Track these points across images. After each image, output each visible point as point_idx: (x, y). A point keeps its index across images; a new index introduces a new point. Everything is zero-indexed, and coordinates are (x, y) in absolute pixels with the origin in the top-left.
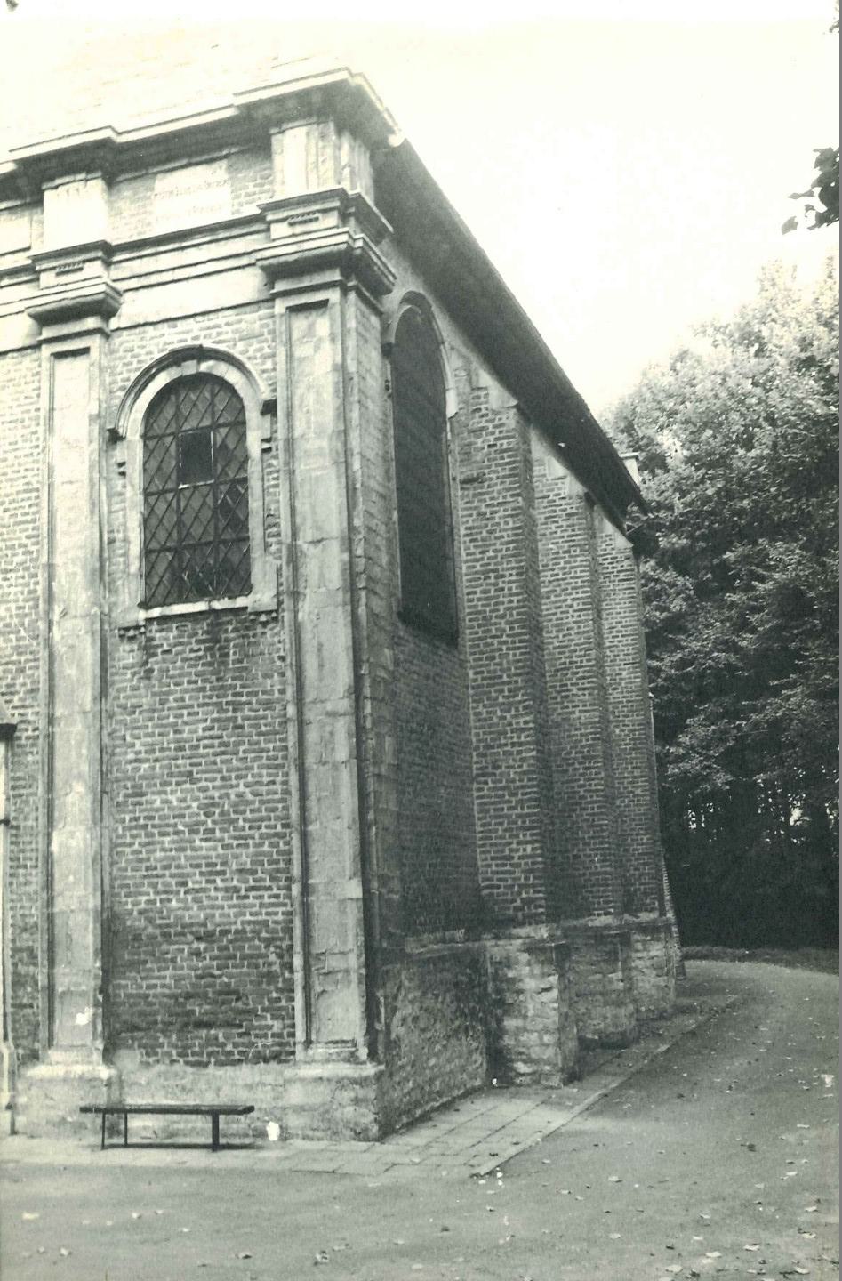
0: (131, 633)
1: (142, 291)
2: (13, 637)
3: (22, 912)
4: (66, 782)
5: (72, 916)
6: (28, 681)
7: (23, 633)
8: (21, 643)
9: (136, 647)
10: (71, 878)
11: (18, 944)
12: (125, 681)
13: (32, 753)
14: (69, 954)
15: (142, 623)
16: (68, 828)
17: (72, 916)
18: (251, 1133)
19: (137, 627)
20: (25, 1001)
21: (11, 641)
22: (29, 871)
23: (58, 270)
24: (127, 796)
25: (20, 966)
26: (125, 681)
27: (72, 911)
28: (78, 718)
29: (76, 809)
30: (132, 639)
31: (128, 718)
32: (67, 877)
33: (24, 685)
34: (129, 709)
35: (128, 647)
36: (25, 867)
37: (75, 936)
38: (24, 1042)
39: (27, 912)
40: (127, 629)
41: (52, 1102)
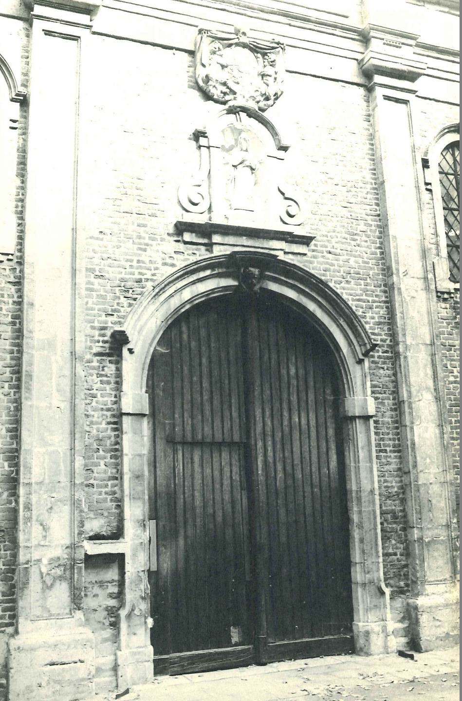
0: (446, 296)
1: (321, 10)
2: (362, 282)
3: (385, 484)
4: (418, 391)
5: (431, 487)
6: (376, 316)
7: (369, 281)
8: (368, 287)
9: (448, 306)
10: (428, 461)
11: (384, 508)
12: (444, 327)
13: (383, 368)
14: (431, 515)
15: (453, 291)
16: (424, 424)
17: (431, 487)
18: (434, 610)
19: (449, 293)
20: (391, 551)
21: (361, 285)
22: (389, 454)
23: (385, 41)
24: (451, 406)
25: (385, 525)
26: (444, 327)
27: (431, 484)
28: (422, 347)
29: (427, 412)
30: (445, 300)
31: (448, 353)
32: (425, 459)
33: (373, 318)
34: (447, 347)
35: (443, 305)
36: (386, 451)
37: (434, 502)
38: (392, 582)
39: (389, 485)
40: (443, 293)
41: (438, 623)
